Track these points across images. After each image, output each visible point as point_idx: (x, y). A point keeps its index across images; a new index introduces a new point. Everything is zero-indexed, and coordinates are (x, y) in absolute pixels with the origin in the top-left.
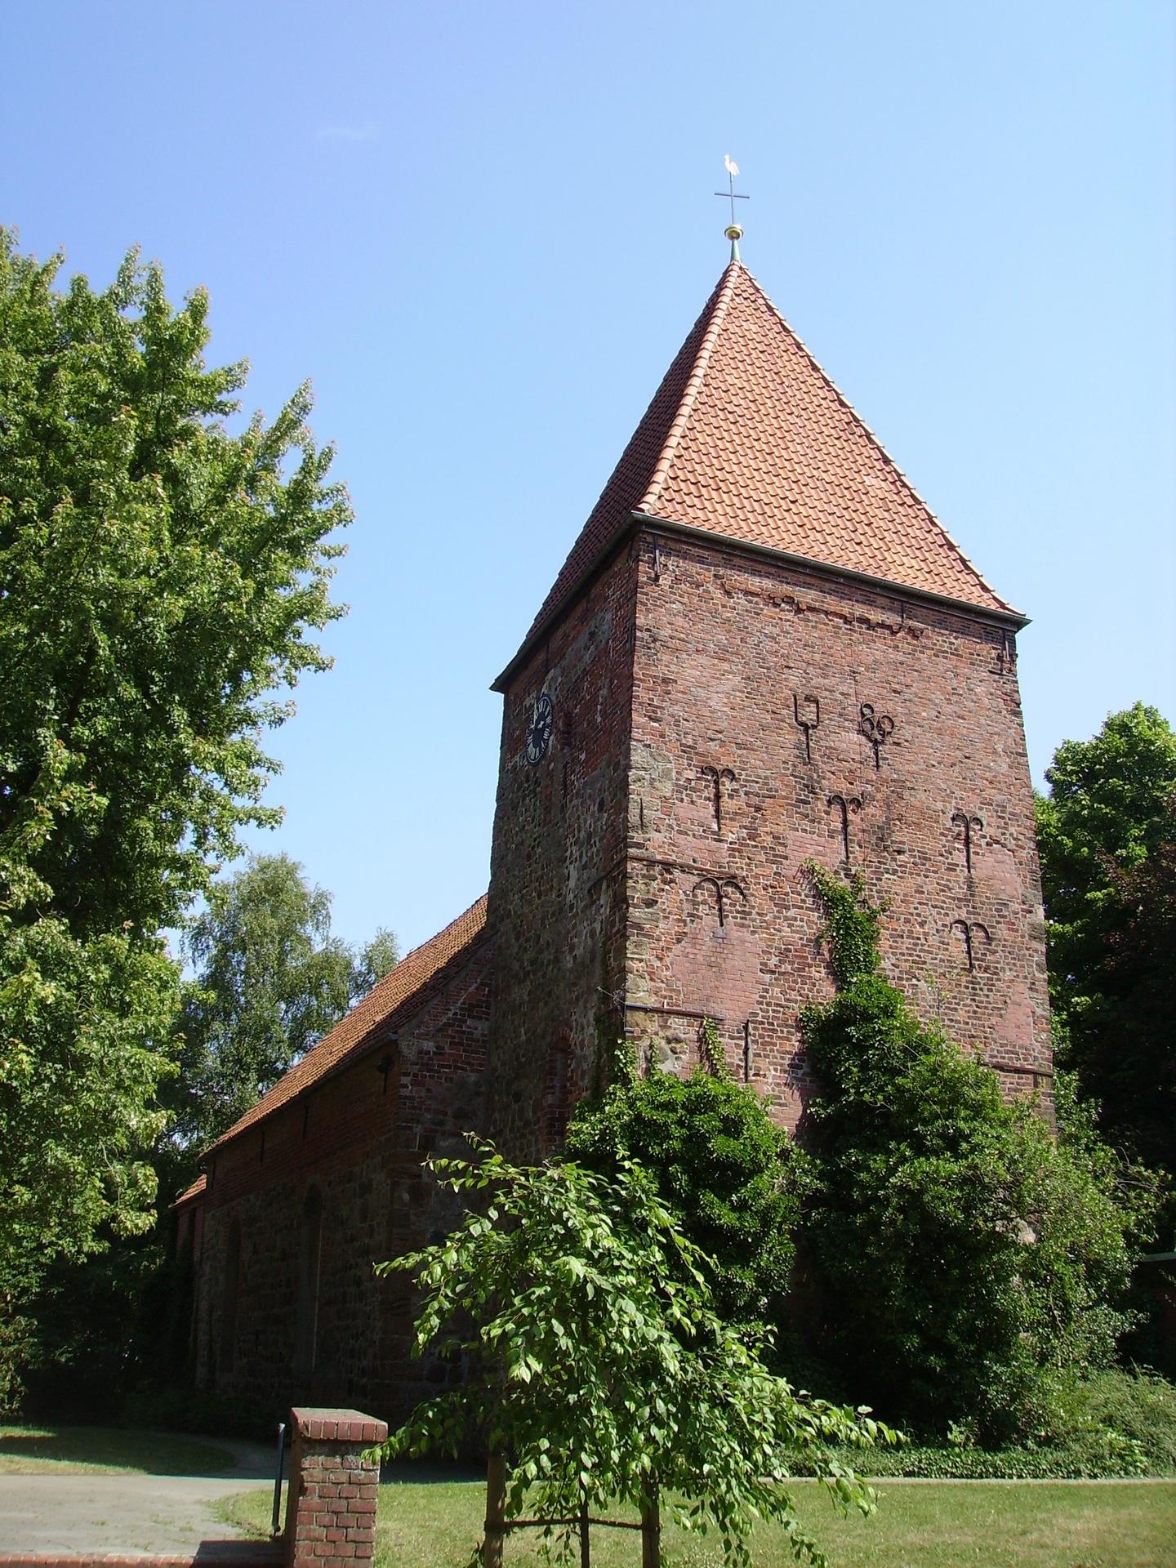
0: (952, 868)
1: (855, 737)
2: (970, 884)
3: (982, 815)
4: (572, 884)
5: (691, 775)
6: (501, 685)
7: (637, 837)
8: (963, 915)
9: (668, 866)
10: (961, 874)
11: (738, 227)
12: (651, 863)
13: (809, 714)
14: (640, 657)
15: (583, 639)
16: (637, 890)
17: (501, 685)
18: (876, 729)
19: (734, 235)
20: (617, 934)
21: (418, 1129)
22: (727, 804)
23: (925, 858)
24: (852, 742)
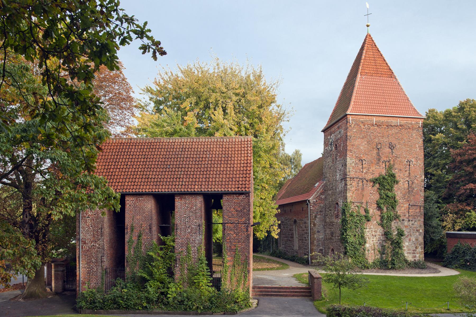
0: (406, 171)
1: (388, 149)
2: (409, 173)
3: (413, 160)
4: (338, 177)
5: (357, 162)
6: (324, 131)
7: (348, 174)
8: (408, 179)
9: (353, 178)
10: (408, 172)
11: (369, 24)
12: (351, 178)
13: (379, 147)
14: (348, 141)
15: (338, 132)
16: (349, 183)
17: (324, 131)
18: (392, 147)
19: (368, 26)
20: (345, 190)
21: (314, 214)
22: (364, 166)
23: (401, 170)
24: (387, 150)
